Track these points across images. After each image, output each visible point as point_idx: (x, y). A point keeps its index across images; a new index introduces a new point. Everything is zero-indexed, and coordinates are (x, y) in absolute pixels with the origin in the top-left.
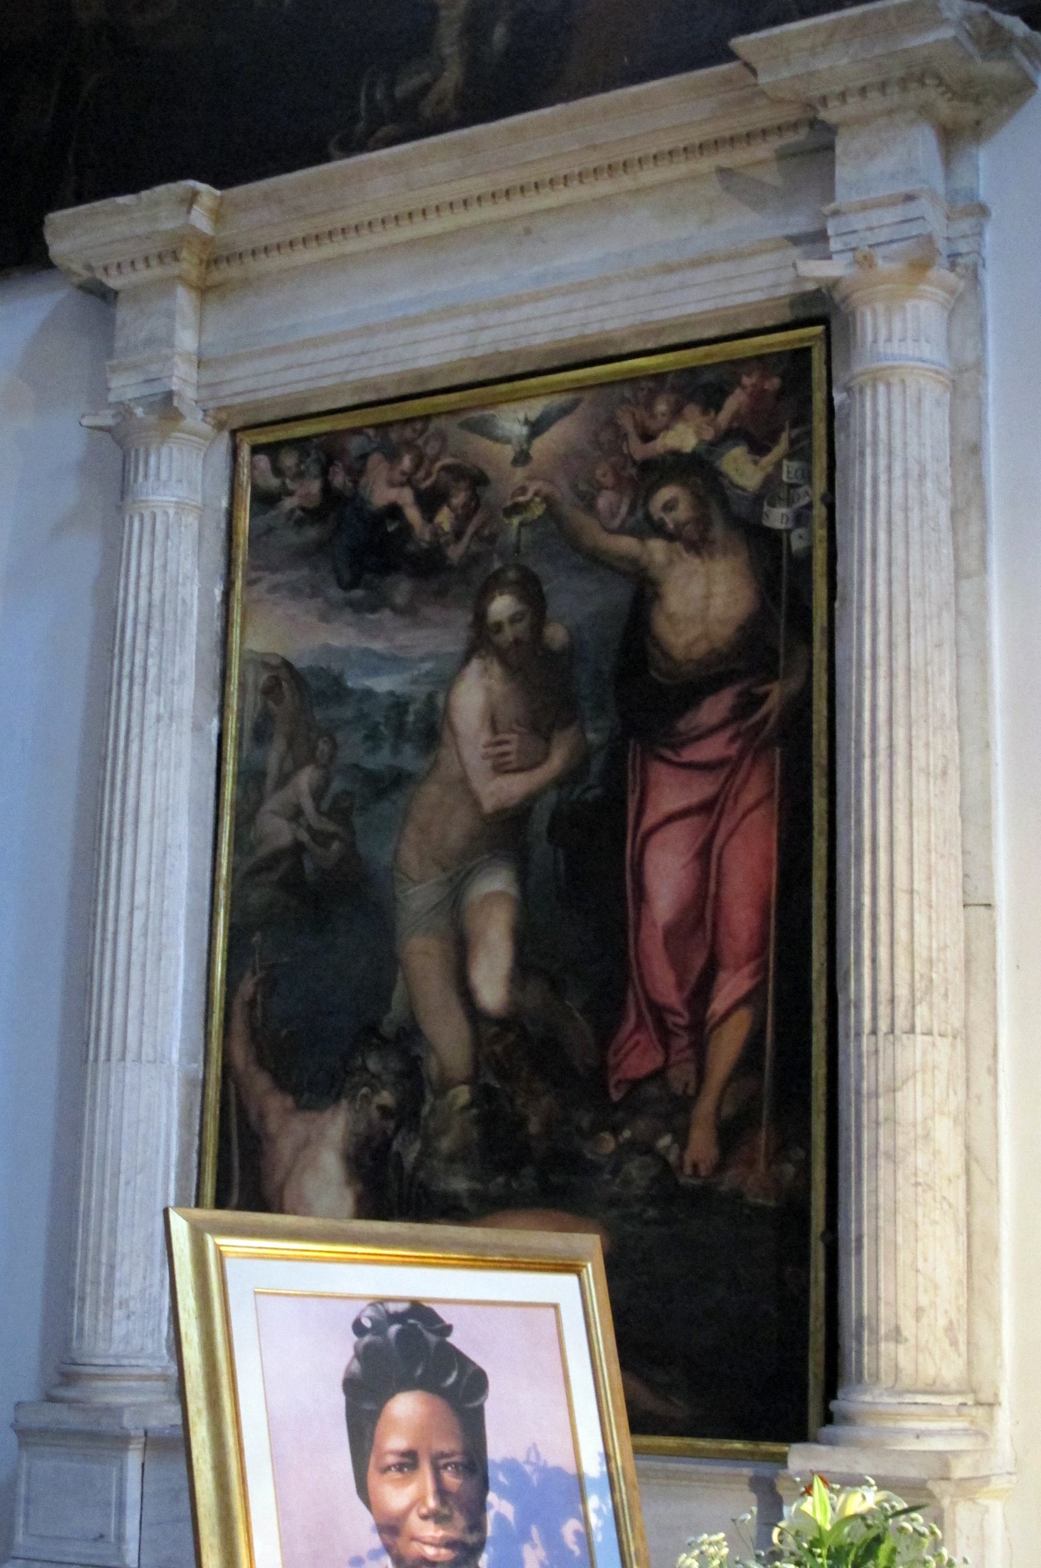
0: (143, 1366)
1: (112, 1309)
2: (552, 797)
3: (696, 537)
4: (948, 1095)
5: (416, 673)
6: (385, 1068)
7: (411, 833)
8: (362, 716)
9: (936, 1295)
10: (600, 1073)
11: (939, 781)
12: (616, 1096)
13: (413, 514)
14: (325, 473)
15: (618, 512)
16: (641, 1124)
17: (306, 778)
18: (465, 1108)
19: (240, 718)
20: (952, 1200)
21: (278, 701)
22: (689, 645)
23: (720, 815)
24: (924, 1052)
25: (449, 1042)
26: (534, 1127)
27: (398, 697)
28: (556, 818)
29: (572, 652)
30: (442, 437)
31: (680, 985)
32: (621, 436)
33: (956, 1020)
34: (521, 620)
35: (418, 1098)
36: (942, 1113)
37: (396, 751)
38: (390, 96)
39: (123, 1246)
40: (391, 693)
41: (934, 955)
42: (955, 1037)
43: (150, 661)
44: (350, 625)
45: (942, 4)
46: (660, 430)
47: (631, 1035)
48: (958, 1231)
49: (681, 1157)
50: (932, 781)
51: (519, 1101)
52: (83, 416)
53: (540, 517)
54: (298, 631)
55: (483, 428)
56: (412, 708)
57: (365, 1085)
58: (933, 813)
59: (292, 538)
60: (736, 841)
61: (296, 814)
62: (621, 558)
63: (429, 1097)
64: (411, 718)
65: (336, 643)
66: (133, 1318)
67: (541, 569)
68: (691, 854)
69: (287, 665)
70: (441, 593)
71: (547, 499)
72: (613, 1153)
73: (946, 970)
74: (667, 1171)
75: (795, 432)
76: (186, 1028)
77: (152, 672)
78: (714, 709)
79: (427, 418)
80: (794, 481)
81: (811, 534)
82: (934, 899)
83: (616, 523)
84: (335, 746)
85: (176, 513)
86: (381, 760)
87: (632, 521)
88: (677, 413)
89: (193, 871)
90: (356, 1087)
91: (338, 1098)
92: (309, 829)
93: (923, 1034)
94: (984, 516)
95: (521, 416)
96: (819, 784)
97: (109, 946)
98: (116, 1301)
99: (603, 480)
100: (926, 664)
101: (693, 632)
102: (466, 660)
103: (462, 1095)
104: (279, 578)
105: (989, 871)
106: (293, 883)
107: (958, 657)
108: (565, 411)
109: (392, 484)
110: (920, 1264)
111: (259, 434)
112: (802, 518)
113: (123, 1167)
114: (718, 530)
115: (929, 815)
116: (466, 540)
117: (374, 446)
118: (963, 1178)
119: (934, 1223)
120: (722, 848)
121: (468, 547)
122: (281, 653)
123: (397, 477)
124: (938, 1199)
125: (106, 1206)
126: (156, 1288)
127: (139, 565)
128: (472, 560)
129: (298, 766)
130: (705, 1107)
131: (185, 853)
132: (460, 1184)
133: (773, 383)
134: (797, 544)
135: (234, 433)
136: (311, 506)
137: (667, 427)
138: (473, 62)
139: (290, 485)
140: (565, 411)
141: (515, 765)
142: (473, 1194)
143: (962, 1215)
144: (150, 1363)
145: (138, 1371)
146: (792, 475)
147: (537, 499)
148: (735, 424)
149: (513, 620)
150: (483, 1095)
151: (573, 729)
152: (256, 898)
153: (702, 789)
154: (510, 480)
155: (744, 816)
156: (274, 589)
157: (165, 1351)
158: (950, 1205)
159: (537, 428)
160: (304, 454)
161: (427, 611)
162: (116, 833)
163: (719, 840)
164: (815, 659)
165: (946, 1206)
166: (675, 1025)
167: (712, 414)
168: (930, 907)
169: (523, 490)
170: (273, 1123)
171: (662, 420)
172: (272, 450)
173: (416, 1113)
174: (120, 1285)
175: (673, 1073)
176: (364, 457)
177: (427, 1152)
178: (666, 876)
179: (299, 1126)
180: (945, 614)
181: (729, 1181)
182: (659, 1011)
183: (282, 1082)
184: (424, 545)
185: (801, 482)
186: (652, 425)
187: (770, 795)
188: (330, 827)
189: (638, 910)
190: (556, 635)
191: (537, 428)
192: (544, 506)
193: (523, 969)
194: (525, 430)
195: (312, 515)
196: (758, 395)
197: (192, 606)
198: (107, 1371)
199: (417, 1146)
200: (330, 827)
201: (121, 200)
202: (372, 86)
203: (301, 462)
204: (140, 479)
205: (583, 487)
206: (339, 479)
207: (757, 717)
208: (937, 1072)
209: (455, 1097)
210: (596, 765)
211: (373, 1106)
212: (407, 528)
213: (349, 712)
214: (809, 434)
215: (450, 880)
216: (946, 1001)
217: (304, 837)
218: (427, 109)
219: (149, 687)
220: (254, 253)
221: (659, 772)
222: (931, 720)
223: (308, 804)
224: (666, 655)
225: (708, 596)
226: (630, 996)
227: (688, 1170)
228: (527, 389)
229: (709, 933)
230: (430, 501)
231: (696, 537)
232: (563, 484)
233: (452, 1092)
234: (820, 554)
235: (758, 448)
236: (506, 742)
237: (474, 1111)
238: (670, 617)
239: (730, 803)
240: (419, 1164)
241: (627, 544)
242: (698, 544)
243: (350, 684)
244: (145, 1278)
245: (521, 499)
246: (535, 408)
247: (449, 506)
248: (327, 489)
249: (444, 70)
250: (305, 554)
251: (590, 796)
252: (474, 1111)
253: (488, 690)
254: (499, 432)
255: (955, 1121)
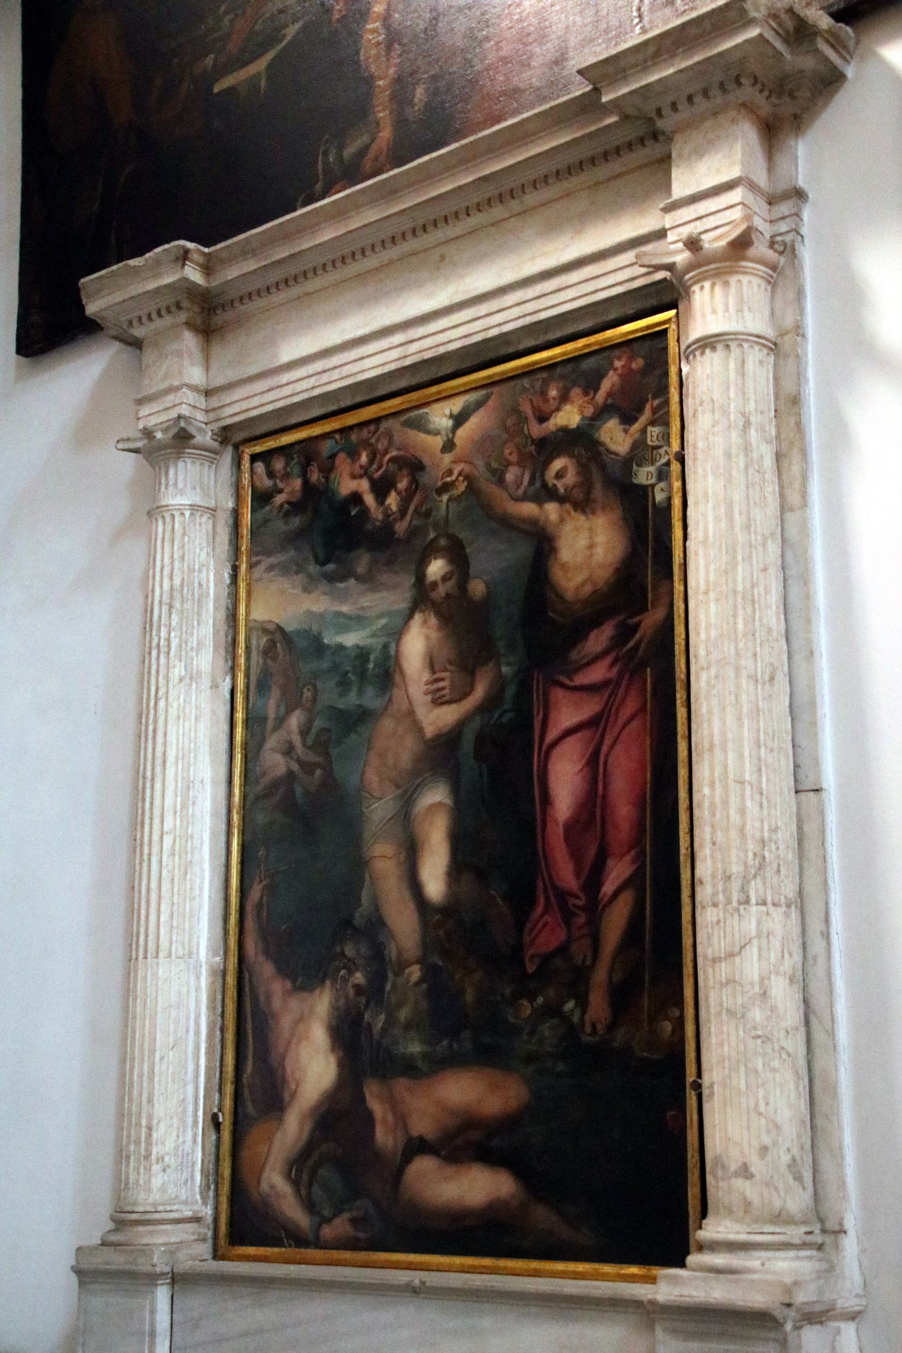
0: (177, 1211)
1: (151, 1165)
2: (476, 723)
3: (581, 497)
4: (783, 956)
5: (374, 628)
6: (358, 953)
7: (373, 758)
8: (335, 667)
9: (778, 1135)
10: (518, 949)
11: (767, 686)
12: (531, 969)
13: (369, 499)
14: (304, 475)
15: (521, 483)
16: (551, 992)
17: (295, 721)
18: (418, 984)
19: (247, 676)
20: (791, 1050)
21: (274, 659)
22: (577, 589)
23: (605, 729)
24: (759, 923)
25: (404, 928)
26: (470, 996)
27: (362, 648)
28: (480, 738)
29: (488, 600)
30: (389, 435)
31: (577, 874)
32: (522, 419)
33: (789, 890)
34: (450, 578)
35: (384, 978)
36: (778, 974)
37: (360, 692)
38: (340, 157)
39: (159, 1110)
40: (357, 646)
41: (766, 835)
42: (788, 906)
43: (173, 634)
44: (325, 593)
45: (748, 6)
46: (553, 412)
47: (542, 916)
48: (798, 1076)
49: (582, 1019)
50: (759, 687)
51: (457, 977)
52: (118, 442)
53: (463, 492)
54: (285, 602)
55: (420, 425)
56: (372, 657)
57: (344, 967)
58: (761, 713)
59: (280, 526)
60: (619, 748)
61: (289, 750)
62: (524, 520)
63: (390, 975)
64: (371, 666)
65: (314, 609)
66: (168, 1171)
67: (464, 535)
68: (584, 761)
69: (280, 629)
70: (389, 562)
71: (468, 477)
72: (531, 1014)
73: (778, 849)
74: (572, 1031)
75: (656, 402)
76: (210, 927)
77: (174, 643)
78: (598, 640)
79: (377, 421)
80: (656, 443)
81: (670, 487)
82: (764, 786)
83: (520, 492)
84: (316, 692)
85: (192, 514)
86: (352, 699)
87: (531, 489)
88: (564, 398)
89: (214, 801)
90: (338, 970)
91: (323, 981)
92: (299, 761)
93: (757, 904)
94: (804, 453)
95: (447, 412)
96: (680, 696)
97: (145, 864)
98: (154, 1157)
99: (510, 458)
100: (753, 586)
101: (580, 578)
102: (410, 616)
103: (415, 972)
104: (272, 560)
105: (816, 762)
106: (289, 805)
107: (785, 580)
108: (479, 404)
109: (354, 477)
110: (762, 1108)
111: (255, 446)
112: (663, 475)
113: (158, 1045)
114: (598, 491)
115: (758, 715)
116: (408, 518)
117: (340, 446)
118: (803, 1029)
119: (773, 1070)
120: (607, 756)
121: (411, 521)
122: (277, 621)
123: (358, 470)
124: (777, 1049)
125: (145, 1078)
126: (189, 1144)
127: (163, 557)
128: (413, 532)
129: (289, 711)
130: (600, 976)
131: (208, 789)
132: (415, 1048)
133: (638, 364)
134: (659, 497)
135: (236, 447)
136: (294, 500)
137: (558, 409)
138: (400, 122)
139: (280, 485)
140: (479, 404)
141: (447, 698)
142: (424, 1056)
143: (802, 1063)
144: (182, 1207)
145: (172, 1216)
146: (654, 439)
147: (461, 478)
148: (610, 401)
149: (445, 579)
150: (431, 972)
151: (491, 664)
152: (261, 818)
153: (589, 708)
154: (441, 464)
155: (623, 727)
156: (270, 568)
157: (198, 1197)
158: (789, 1055)
159: (459, 419)
160: (289, 458)
161: (384, 578)
162: (149, 774)
163: (605, 748)
164: (675, 591)
165: (784, 1056)
166: (574, 905)
167: (592, 393)
168: (761, 794)
169: (450, 472)
170: (277, 1003)
171: (553, 404)
172: (264, 457)
173: (381, 989)
174: (156, 1144)
175: (574, 948)
176: (333, 457)
177: (391, 1022)
178: (565, 781)
179: (295, 1005)
180: (769, 541)
181: (620, 1036)
182: (562, 895)
183: (285, 970)
184: (378, 523)
185: (661, 443)
186: (546, 408)
187: (643, 709)
188: (312, 757)
189: (544, 813)
190: (477, 588)
191: (459, 419)
192: (466, 483)
193: (457, 868)
194: (450, 423)
195: (295, 507)
196: (627, 375)
197: (208, 588)
198: (148, 1216)
199: (382, 1017)
200: (312, 757)
201: (133, 262)
202: (325, 153)
203: (287, 464)
204: (163, 489)
205: (495, 465)
206: (315, 476)
207: (631, 644)
208: (771, 938)
209: (410, 974)
210: (511, 691)
211: (350, 985)
212: (365, 511)
213: (325, 665)
214: (667, 402)
215: (403, 794)
216: (779, 876)
217: (295, 767)
218: (367, 165)
219: (172, 654)
220: (241, 299)
221: (558, 695)
222: (757, 634)
223: (297, 740)
224: (561, 597)
225: (591, 547)
226: (540, 884)
227: (588, 1030)
228: (452, 388)
229: (599, 828)
230: (381, 488)
231: (581, 497)
232: (480, 463)
233: (407, 971)
234: (677, 502)
235: (628, 419)
236: (442, 679)
237: (424, 986)
238: (564, 567)
239: (611, 720)
240: (384, 1031)
241: (529, 509)
242: (581, 502)
243: (326, 641)
244: (178, 1137)
245: (449, 479)
246: (457, 405)
247: (396, 490)
248: (306, 483)
249: (379, 132)
250: (293, 539)
251: (504, 720)
252: (424, 986)
253: (427, 638)
254: (431, 426)
255: (792, 980)
